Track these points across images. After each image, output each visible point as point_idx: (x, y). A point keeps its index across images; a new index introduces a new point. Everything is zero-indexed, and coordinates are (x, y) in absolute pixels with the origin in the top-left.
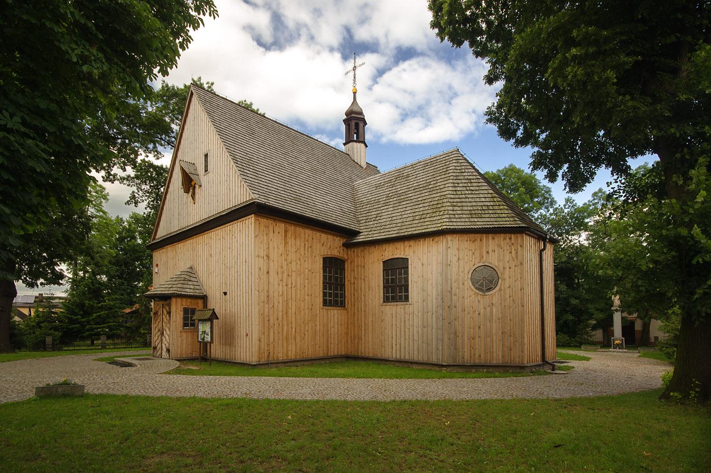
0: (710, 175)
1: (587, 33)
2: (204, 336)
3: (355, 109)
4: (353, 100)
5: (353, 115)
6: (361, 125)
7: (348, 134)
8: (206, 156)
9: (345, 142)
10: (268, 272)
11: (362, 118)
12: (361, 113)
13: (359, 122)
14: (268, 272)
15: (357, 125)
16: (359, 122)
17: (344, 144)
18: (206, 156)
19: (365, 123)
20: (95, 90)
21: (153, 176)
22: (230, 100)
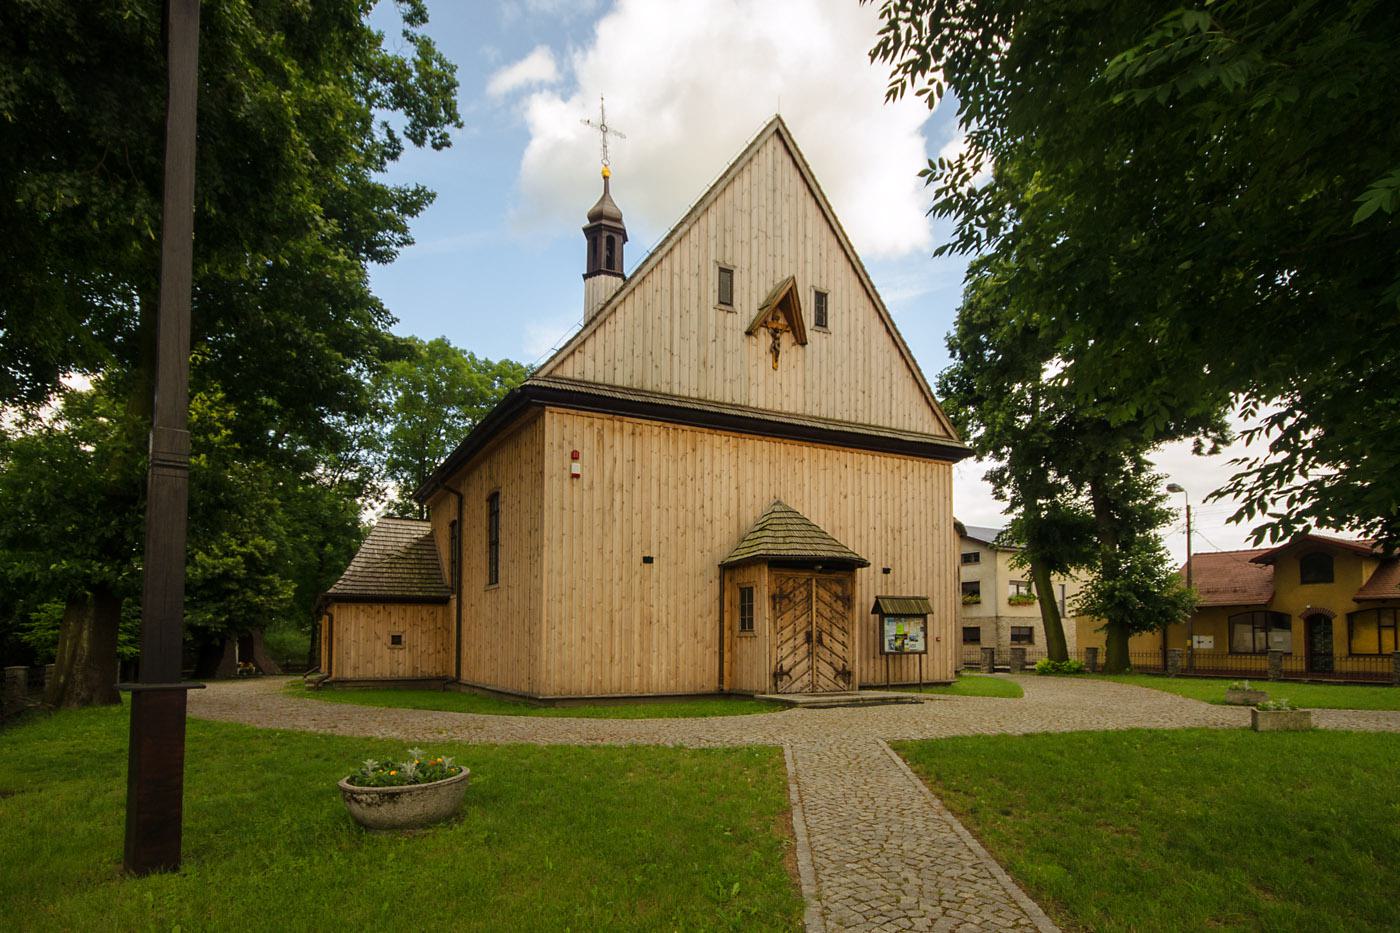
0: (1379, 385)
1: (411, 76)
2: (903, 643)
3: (607, 209)
4: (603, 193)
5: (604, 222)
6: (618, 239)
7: (592, 252)
8: (1204, 501)
9: (585, 272)
10: (711, 499)
11: (620, 229)
12: (619, 220)
13: (615, 236)
14: (711, 499)
15: (611, 242)
16: (615, 236)
17: (584, 275)
18: (1204, 501)
19: (625, 239)
20: (18, 266)
21: (127, 514)
22: (717, 179)
